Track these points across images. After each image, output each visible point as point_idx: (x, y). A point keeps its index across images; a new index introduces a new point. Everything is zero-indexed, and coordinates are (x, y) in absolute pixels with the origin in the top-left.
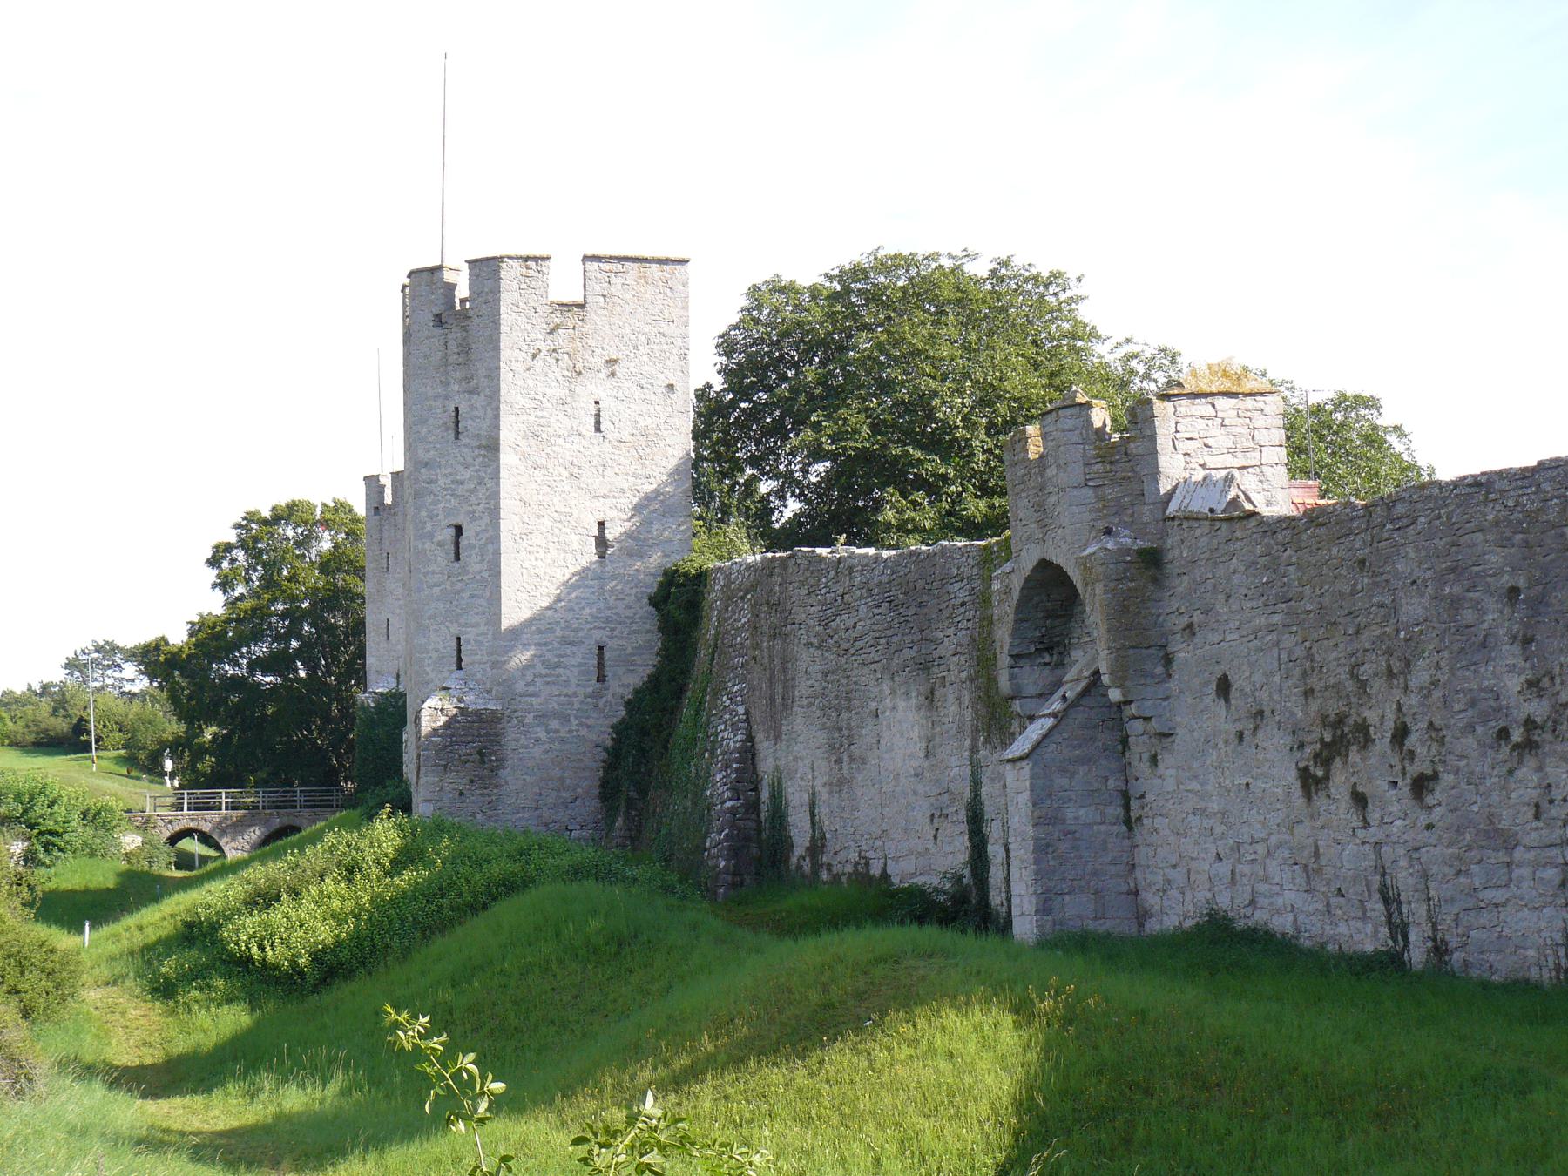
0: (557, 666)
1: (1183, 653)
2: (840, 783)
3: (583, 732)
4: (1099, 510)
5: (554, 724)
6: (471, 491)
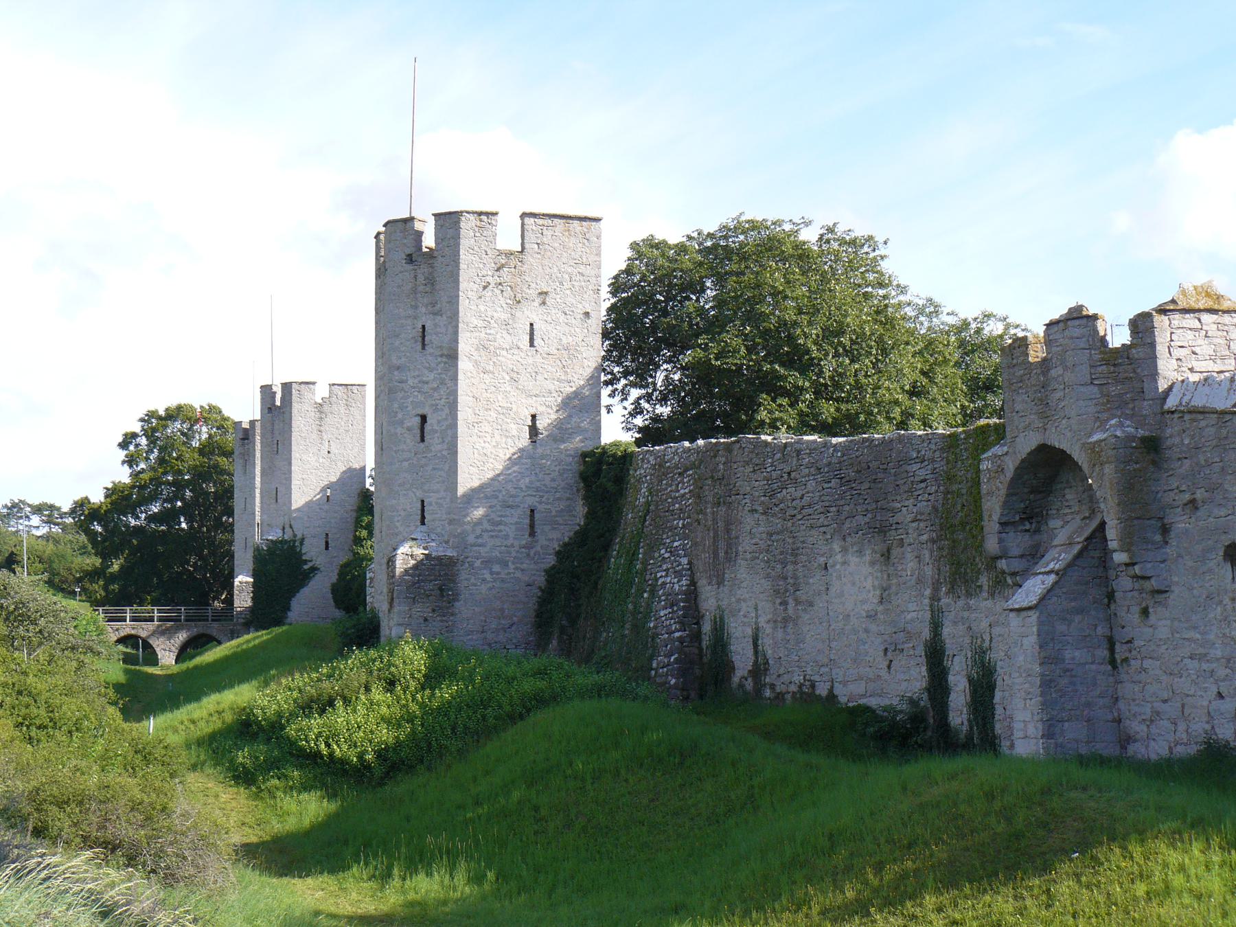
0: (500, 523)
1: (1181, 523)
2: (786, 620)
3: (518, 574)
4: (1103, 404)
5: (496, 568)
6: (435, 389)
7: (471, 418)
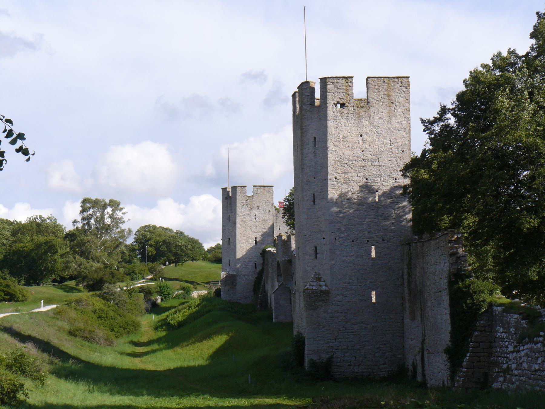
5: (246, 277)
7: (240, 239)
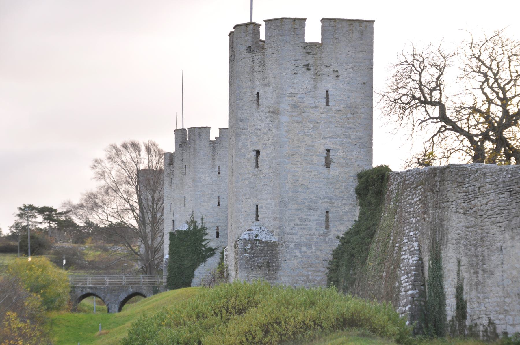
0: (306, 220)
2: (477, 284)
5: (304, 249)
6: (265, 134)
